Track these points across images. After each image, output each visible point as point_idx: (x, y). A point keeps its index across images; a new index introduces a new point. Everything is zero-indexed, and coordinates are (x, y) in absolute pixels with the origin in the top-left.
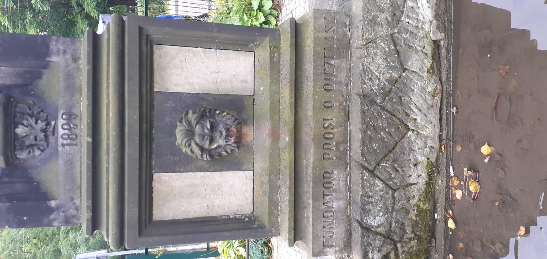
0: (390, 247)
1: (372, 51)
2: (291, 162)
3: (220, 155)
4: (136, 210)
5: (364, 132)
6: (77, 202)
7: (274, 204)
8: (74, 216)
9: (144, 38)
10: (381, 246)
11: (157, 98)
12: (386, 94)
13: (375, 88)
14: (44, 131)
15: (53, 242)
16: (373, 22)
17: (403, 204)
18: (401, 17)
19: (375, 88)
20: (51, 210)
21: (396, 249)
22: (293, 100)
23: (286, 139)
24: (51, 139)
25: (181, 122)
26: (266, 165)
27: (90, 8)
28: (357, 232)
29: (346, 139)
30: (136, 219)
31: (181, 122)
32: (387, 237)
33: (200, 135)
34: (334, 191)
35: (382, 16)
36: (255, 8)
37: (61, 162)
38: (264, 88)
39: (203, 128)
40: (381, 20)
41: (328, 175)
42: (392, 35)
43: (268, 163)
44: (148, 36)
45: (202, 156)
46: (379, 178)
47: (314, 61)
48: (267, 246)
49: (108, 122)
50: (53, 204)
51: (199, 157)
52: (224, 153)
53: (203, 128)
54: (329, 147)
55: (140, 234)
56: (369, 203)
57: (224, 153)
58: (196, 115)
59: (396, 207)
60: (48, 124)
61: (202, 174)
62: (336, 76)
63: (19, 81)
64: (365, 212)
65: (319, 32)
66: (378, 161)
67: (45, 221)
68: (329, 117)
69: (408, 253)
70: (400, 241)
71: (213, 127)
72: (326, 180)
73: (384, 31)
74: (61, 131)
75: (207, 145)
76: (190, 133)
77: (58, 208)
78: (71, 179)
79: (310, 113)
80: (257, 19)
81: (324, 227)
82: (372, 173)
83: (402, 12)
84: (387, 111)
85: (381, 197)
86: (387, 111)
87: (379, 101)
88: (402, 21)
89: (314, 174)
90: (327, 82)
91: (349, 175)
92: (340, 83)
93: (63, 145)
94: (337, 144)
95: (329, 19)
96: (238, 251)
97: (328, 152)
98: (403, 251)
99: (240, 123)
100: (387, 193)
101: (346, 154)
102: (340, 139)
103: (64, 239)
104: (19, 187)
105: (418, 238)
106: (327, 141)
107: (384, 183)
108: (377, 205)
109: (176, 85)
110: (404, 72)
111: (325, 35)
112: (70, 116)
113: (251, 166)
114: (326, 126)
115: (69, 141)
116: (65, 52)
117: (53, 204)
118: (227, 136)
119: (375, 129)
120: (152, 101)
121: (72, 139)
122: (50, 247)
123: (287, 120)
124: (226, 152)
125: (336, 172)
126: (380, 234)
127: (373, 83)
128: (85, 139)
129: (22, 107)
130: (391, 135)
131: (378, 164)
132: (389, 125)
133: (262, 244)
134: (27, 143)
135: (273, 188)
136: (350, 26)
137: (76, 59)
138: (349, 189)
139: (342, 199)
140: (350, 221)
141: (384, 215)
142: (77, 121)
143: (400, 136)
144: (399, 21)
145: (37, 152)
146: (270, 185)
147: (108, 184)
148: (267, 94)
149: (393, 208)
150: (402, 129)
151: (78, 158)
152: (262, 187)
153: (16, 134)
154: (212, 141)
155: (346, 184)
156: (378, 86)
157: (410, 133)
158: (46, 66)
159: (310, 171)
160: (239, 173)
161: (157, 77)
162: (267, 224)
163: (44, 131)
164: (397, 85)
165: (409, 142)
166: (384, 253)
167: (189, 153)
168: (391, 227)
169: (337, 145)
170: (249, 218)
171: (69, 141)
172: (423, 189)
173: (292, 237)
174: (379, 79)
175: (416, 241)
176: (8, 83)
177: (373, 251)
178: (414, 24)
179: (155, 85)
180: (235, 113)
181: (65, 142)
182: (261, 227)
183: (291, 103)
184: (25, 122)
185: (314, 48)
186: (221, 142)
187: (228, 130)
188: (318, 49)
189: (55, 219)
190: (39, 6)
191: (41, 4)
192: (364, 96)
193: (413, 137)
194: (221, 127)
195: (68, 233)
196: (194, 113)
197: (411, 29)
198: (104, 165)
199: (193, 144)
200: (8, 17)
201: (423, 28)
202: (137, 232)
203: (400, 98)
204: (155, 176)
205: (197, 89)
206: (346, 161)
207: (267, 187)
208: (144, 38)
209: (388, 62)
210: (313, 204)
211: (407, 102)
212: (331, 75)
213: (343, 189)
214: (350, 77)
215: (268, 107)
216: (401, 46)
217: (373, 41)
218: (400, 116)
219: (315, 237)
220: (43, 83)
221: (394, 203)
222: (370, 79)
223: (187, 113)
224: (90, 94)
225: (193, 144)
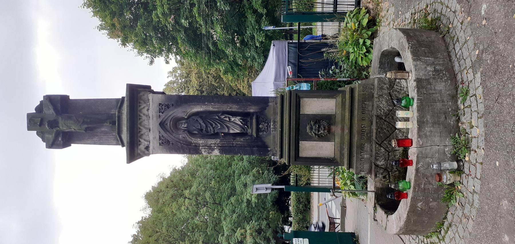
0: (386, 173)
1: (381, 99)
2: (348, 139)
3: (322, 136)
4: (294, 153)
5: (377, 130)
6: (276, 149)
7: (342, 155)
8: (275, 153)
9: (298, 97)
10: (383, 173)
11: (301, 116)
12: (387, 115)
13: (382, 113)
14: (267, 126)
15: (230, 182)
16: (381, 88)
17: (392, 158)
18: (394, 86)
19: (382, 113)
20: (269, 151)
21: (389, 174)
22: (350, 117)
23: (347, 131)
24: (269, 129)
25: (309, 125)
26: (339, 140)
27: (257, 5)
28: (373, 166)
29: (371, 132)
30: (294, 155)
31: (309, 125)
32: (385, 169)
33: (315, 129)
34: (365, 151)
35: (385, 86)
36: (361, 44)
37: (272, 136)
38: (339, 112)
39: (316, 127)
40: (385, 87)
41: (363, 145)
42: (390, 93)
43: (340, 140)
44: (299, 96)
45: (315, 136)
46: (383, 147)
47: (358, 103)
48: (365, 185)
49: (286, 124)
50: (269, 149)
51: (314, 137)
52: (323, 135)
53: (316, 127)
54: (364, 134)
55: (295, 160)
56: (378, 156)
57: (323, 135)
58: (313, 123)
59: (390, 158)
60: (268, 124)
61: (316, 142)
62: (367, 108)
63: (260, 111)
64: (377, 160)
65: (360, 92)
66: (382, 141)
67: (267, 154)
68: (364, 124)
69: (394, 176)
70: (391, 171)
71: (319, 127)
72: (362, 147)
73: (386, 91)
74: (272, 127)
75: (317, 133)
76: (311, 129)
77: (271, 150)
78: (274, 142)
79: (356, 122)
80: (362, 50)
81: (361, 164)
82: (380, 145)
83: (394, 84)
84: (387, 122)
85: (383, 154)
86: (387, 122)
87: (384, 118)
88: (394, 87)
89: (357, 144)
90: (363, 110)
91: (372, 145)
92: (368, 111)
93: (272, 131)
94: (367, 133)
95: (365, 87)
96: (350, 188)
97: (363, 136)
98: (392, 175)
99: (330, 125)
100: (386, 153)
101: (371, 138)
102: (368, 132)
103: (238, 180)
104: (260, 143)
105: (399, 171)
106: (363, 133)
107: (385, 149)
108: (381, 157)
109: (307, 111)
110: (395, 107)
111: (363, 93)
112: (274, 122)
113: (334, 140)
114: (362, 127)
115: (274, 130)
116: (273, 101)
117: (269, 149)
118: (324, 130)
119: (381, 128)
120: (299, 117)
121: (275, 129)
122: (229, 185)
123: (347, 124)
124: (324, 135)
125: (366, 144)
126: (383, 168)
127: (381, 111)
128: (279, 129)
129: (261, 119)
130: (388, 131)
131: (383, 142)
132: (387, 127)
133: (363, 183)
134: (262, 130)
135: (342, 149)
136: (373, 89)
137: (276, 104)
138: (372, 151)
139: (368, 154)
140: (371, 163)
141: (384, 161)
142: (276, 123)
143: (392, 132)
144: (393, 87)
145: (265, 133)
146: (340, 148)
147: (286, 144)
148: (340, 114)
149: (388, 159)
150: (393, 129)
151: (277, 135)
152: (337, 148)
153: (259, 127)
154: (319, 131)
155: (370, 149)
156: (383, 112)
157: (397, 130)
158: (268, 106)
159: (355, 143)
160: (329, 143)
161: (301, 109)
162: (339, 161)
163: (267, 126)
164: (392, 112)
165: (396, 134)
166: (384, 175)
167: (311, 134)
168: (387, 166)
169: (367, 134)
170: (333, 159)
171: (274, 130)
172: (402, 152)
173: (348, 167)
174: (384, 110)
175: (398, 172)
176: (257, 111)
177: (379, 174)
178: (400, 88)
179: (301, 112)
180: (328, 121)
181: (273, 130)
182: (337, 162)
183: (349, 118)
184: (262, 124)
185: (358, 98)
186: (322, 132)
187: (324, 128)
188: (360, 98)
189: (270, 154)
190: (222, 7)
191: (224, 6)
192: (377, 116)
193: (398, 132)
194: (322, 127)
195: (240, 175)
196: (313, 122)
197: (398, 90)
198: (284, 138)
199: (312, 132)
200: (203, 18)
201: (403, 90)
202: (294, 160)
203: (393, 117)
204: (300, 142)
205: (314, 113)
206: (371, 140)
207: (339, 148)
208: (298, 97)
209: (388, 103)
210: (356, 155)
211: (396, 118)
212: (365, 108)
213: (369, 151)
214: (373, 108)
215: (340, 119)
216: (394, 97)
217: (382, 95)
218: (392, 124)
219: (357, 168)
220: (266, 111)
221: (389, 157)
222: (380, 110)
223: (311, 121)
224: (281, 115)
225: (312, 132)
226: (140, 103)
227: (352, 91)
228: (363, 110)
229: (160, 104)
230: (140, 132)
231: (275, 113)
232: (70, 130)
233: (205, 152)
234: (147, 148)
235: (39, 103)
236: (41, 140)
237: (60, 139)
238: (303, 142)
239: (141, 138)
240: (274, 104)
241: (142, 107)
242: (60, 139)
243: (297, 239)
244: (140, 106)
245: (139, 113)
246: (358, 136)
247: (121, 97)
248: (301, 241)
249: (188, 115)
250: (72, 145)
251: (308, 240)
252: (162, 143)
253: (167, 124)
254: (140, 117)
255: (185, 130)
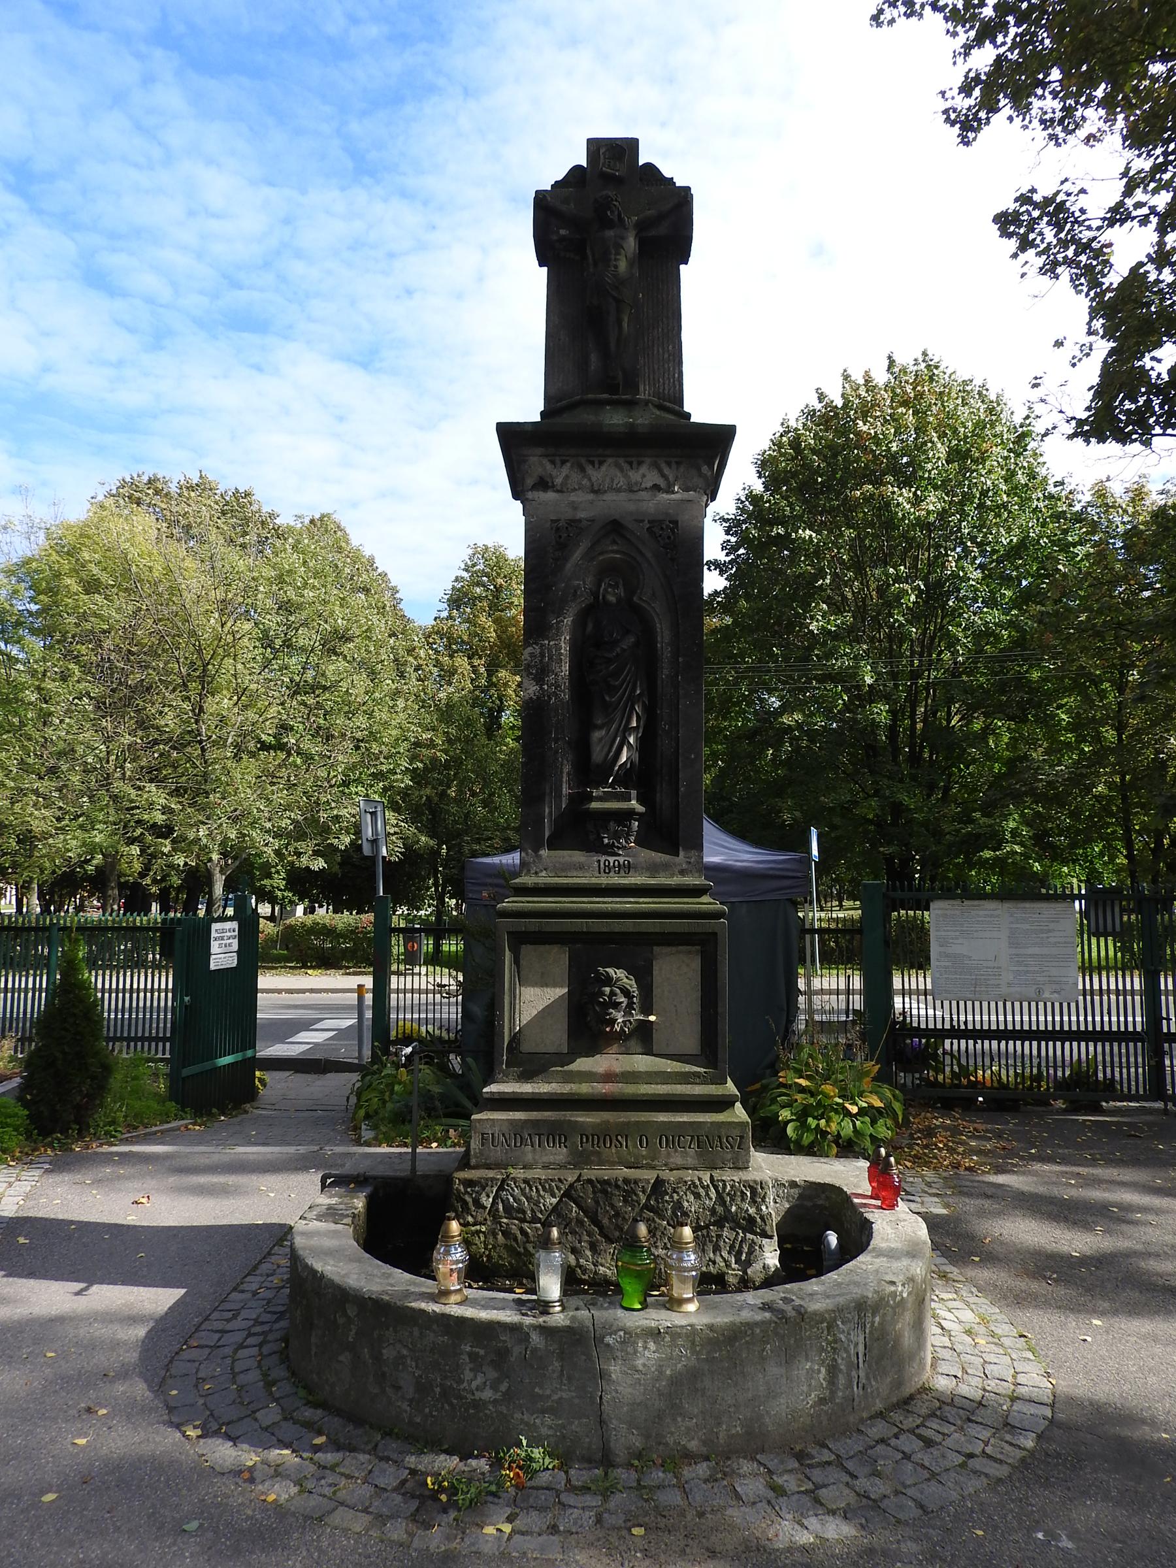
77: (539, 857)
82: (566, 1194)
93: (599, 861)
128: (604, 880)
155: (550, 1163)
226: (678, 463)
227: (724, 1104)
228: (673, 1136)
229: (676, 523)
230: (592, 463)
231: (564, 869)
232: (591, 260)
233: (532, 655)
234: (543, 484)
235: (667, 174)
236: (560, 178)
237: (563, 232)
238: (565, 958)
239: (572, 466)
240: (680, 864)
241: (666, 471)
242: (563, 232)
243: (236, 933)
244: (669, 464)
245: (648, 460)
246: (593, 1125)
247: (686, 408)
248: (230, 945)
249: (644, 605)
250: (545, 269)
251: (234, 965)
252: (558, 529)
253: (614, 542)
254: (635, 465)
255: (596, 597)
